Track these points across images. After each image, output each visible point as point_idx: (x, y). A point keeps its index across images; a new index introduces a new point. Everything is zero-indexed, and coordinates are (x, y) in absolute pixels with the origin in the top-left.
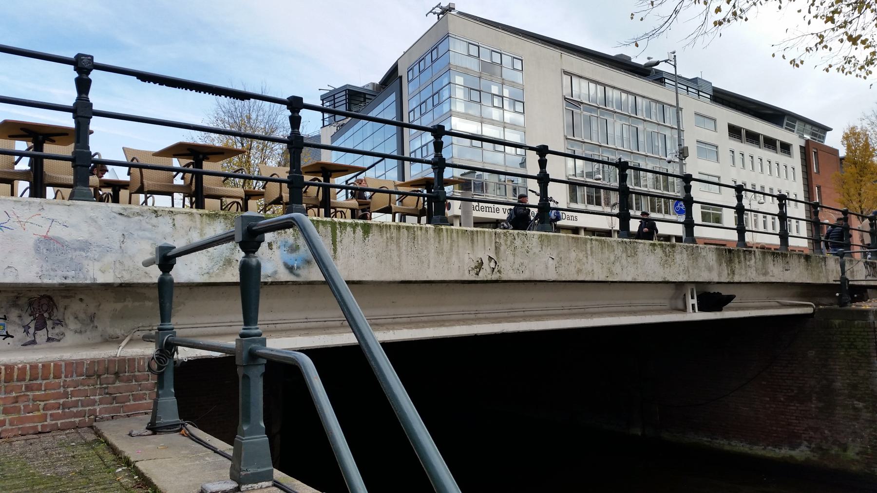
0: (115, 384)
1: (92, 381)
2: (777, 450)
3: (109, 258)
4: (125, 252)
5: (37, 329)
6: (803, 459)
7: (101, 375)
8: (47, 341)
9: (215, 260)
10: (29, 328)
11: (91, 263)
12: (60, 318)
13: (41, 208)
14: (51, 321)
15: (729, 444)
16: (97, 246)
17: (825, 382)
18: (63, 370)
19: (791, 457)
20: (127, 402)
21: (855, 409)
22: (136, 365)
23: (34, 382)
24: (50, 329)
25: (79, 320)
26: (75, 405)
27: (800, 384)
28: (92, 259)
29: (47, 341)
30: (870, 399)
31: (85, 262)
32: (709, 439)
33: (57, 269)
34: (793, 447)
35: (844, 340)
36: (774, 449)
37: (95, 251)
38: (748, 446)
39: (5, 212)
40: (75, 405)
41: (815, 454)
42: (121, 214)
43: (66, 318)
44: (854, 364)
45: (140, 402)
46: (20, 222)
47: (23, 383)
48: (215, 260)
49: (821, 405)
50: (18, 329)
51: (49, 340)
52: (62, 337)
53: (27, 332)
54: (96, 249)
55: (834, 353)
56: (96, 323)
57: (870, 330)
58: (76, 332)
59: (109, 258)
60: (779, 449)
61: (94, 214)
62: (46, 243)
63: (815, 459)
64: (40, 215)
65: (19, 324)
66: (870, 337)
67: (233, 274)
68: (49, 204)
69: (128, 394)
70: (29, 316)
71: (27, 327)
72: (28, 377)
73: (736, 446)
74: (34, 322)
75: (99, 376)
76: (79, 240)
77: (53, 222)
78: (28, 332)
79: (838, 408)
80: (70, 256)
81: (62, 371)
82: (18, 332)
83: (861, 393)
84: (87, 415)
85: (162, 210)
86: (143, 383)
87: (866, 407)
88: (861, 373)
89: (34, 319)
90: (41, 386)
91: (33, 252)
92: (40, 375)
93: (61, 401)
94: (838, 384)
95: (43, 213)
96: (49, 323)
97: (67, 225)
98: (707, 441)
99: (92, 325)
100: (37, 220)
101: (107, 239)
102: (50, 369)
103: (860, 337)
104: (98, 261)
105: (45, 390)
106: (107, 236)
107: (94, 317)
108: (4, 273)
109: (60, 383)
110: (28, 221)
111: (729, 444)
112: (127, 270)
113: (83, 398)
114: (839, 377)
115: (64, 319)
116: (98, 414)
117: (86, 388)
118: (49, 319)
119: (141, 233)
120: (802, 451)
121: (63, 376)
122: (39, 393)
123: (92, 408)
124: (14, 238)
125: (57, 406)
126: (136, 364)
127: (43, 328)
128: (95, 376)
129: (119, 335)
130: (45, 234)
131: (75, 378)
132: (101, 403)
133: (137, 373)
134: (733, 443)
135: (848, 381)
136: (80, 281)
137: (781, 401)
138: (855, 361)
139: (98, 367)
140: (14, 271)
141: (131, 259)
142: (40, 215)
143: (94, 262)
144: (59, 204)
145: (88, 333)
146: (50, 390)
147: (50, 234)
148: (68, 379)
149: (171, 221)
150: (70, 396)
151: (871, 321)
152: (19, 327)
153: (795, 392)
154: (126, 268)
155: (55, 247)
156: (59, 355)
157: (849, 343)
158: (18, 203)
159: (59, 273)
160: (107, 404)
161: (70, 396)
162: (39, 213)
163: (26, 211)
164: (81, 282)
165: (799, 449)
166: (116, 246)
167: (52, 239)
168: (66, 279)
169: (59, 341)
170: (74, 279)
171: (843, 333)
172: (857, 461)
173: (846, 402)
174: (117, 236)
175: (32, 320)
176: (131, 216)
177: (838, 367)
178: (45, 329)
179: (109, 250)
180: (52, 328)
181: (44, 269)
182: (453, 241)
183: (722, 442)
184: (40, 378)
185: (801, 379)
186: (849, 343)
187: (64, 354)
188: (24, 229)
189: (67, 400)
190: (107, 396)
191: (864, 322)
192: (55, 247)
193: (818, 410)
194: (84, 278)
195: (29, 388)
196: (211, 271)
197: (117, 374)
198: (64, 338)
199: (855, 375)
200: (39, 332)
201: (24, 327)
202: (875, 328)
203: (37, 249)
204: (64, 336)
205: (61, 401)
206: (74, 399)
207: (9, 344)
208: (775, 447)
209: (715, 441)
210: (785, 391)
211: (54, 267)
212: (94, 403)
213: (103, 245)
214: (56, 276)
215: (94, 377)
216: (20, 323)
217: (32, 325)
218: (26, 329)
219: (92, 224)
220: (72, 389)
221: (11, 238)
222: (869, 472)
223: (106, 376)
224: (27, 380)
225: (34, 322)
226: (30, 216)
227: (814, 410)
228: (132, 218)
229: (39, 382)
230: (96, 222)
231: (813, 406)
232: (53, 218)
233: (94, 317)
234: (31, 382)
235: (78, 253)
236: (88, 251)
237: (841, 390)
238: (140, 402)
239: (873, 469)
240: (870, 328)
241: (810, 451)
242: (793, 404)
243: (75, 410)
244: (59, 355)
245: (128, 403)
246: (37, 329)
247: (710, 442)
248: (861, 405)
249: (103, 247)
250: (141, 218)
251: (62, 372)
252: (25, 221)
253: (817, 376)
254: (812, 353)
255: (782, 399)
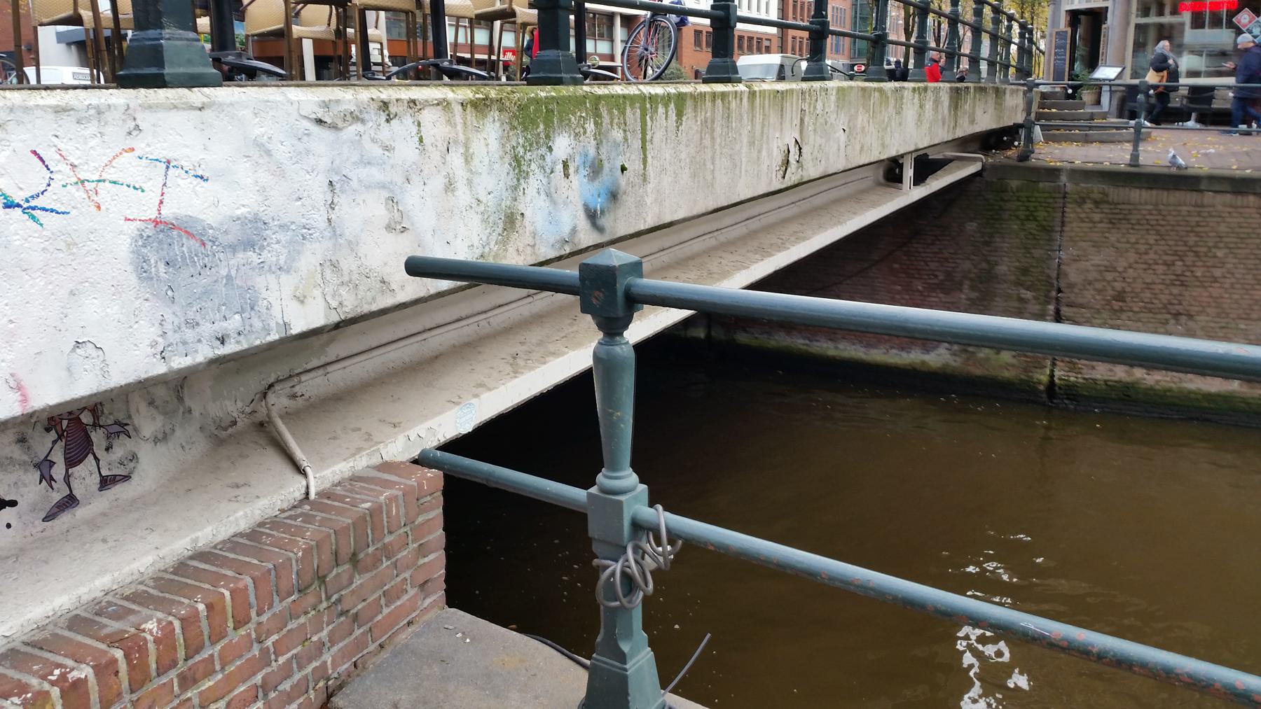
0: (353, 582)
1: (311, 599)
2: (904, 354)
3: (309, 259)
4: (338, 233)
5: (72, 462)
6: (939, 365)
7: (325, 577)
8: (101, 489)
9: (491, 219)
10: (52, 464)
11: (272, 279)
12: (121, 417)
13: (132, 124)
14: (100, 432)
15: (836, 348)
16: (280, 226)
17: (984, 265)
18: (252, 599)
19: (923, 362)
20: (376, 616)
21: (1021, 300)
22: (385, 520)
23: (198, 658)
24: (100, 453)
25: (157, 407)
26: (287, 672)
27: (948, 267)
28: (273, 268)
29: (101, 489)
30: (1043, 288)
31: (260, 282)
32: (807, 342)
33: (198, 318)
34: (927, 350)
35: (1022, 208)
36: (899, 353)
37: (278, 242)
38: (863, 349)
39: (34, 152)
40: (287, 672)
41: (957, 359)
42: (320, 122)
43: (133, 411)
44: (1029, 241)
45: (398, 603)
46: (83, 182)
47: (173, 674)
48: (491, 219)
49: (974, 295)
50: (23, 477)
51: (106, 482)
52: (132, 465)
53: (47, 478)
54: (280, 236)
55: (1004, 226)
56: (188, 402)
57: (1057, 195)
58: (156, 441)
59: (309, 259)
60: (908, 352)
61: (263, 130)
62: (160, 242)
63: (954, 364)
64: (133, 150)
65: (23, 464)
66: (1058, 205)
67: (518, 250)
68: (150, 107)
69: (376, 595)
70: (45, 434)
71: (46, 466)
72: (181, 654)
73: (846, 350)
74: (61, 444)
75: (322, 579)
76: (239, 219)
77: (168, 168)
78: (51, 476)
79: (997, 299)
80: (224, 272)
81: (250, 604)
82: (25, 485)
83: (1032, 279)
84: (311, 685)
85: (397, 100)
86: (399, 556)
87: (1035, 298)
88: (1037, 253)
89: (60, 437)
90: (213, 661)
91: (133, 279)
92: (206, 633)
93: (258, 679)
94: (1002, 269)
95: (140, 145)
96: (97, 437)
97: (206, 175)
98: (804, 345)
99: (181, 411)
100: (128, 168)
101: (299, 203)
102: (224, 607)
103: (1044, 204)
104: (288, 271)
105: (223, 669)
106: (295, 197)
107: (182, 388)
108: (68, 369)
109: (249, 635)
110: (105, 176)
111: (836, 348)
112: (161, 222)
113: (300, 648)
114: (1006, 259)
115: (130, 417)
116: (330, 672)
117: (302, 620)
118: (96, 425)
119: (363, 172)
120: (939, 355)
121: (253, 613)
122: (211, 683)
123: (318, 664)
124: (76, 244)
125: (253, 693)
126: (385, 516)
127: (86, 456)
128: (316, 583)
129: (235, 414)
130: (153, 214)
131: (278, 607)
132: (333, 642)
133: (388, 539)
134: (841, 346)
135: (1017, 264)
136: (256, 338)
137: (918, 291)
138: (1030, 237)
139: (319, 558)
140: (94, 352)
141: (352, 250)
142: (133, 150)
143: (278, 278)
144: (175, 107)
145: (178, 432)
146: (230, 662)
147: (167, 212)
148: (264, 618)
149: (414, 129)
150: (273, 657)
151: (1062, 184)
152: (26, 471)
153: (941, 278)
154: (346, 279)
155: (185, 249)
156: (188, 539)
157: (1027, 213)
158: (64, 116)
159: (207, 329)
160: (344, 639)
161: (273, 657)
162: (129, 143)
163: (93, 143)
164: (258, 342)
165: (936, 352)
166: (319, 220)
167: (174, 227)
168: (223, 343)
169: (126, 478)
170: (241, 338)
171: (1154, 232)
172: (1013, 366)
173: (1010, 291)
174: (319, 193)
175: (54, 442)
176: (340, 125)
177: (1006, 245)
178: (91, 457)
179: (305, 233)
180: (107, 449)
181: (168, 327)
182: (764, 115)
183: (825, 345)
184: (207, 643)
185: (951, 261)
186: (1027, 213)
187: (199, 534)
188: (99, 207)
189: (269, 670)
190: (343, 619)
191: (1052, 184)
192: (185, 249)
193: (969, 302)
194: (264, 328)
195: (187, 681)
196: (487, 250)
197: (354, 559)
198: (138, 465)
199: (1028, 255)
200: (77, 471)
201: (37, 466)
202: (1066, 193)
203: (142, 269)
204: (137, 462)
205: (258, 679)
206: (282, 660)
207: (9, 526)
208: (903, 349)
209: (815, 343)
210: (926, 277)
211: (191, 315)
212: (321, 647)
213: (293, 223)
214: (199, 341)
215: (314, 587)
216: (25, 458)
217: (58, 457)
218: (44, 468)
219: (261, 161)
220: (275, 637)
221: (68, 245)
222: (1026, 378)
223: (334, 572)
224: (181, 663)
225: (61, 444)
226: (105, 160)
227: (964, 301)
228: (345, 130)
229: (205, 654)
230: (268, 153)
231: (963, 296)
232: (170, 155)
233: (182, 388)
234: (190, 662)
235: (241, 256)
236: (262, 248)
237: (1005, 275)
238: (398, 603)
239: (1030, 374)
240: (1059, 193)
241: (951, 355)
242: (934, 294)
243: (286, 686)
244: (188, 539)
245: (380, 617)
246: (72, 462)
247: (807, 345)
248: (1028, 295)
249: (293, 227)
250: (358, 127)
251: (250, 606)
252: (96, 177)
253: (974, 257)
254: (972, 226)
255: (920, 288)
